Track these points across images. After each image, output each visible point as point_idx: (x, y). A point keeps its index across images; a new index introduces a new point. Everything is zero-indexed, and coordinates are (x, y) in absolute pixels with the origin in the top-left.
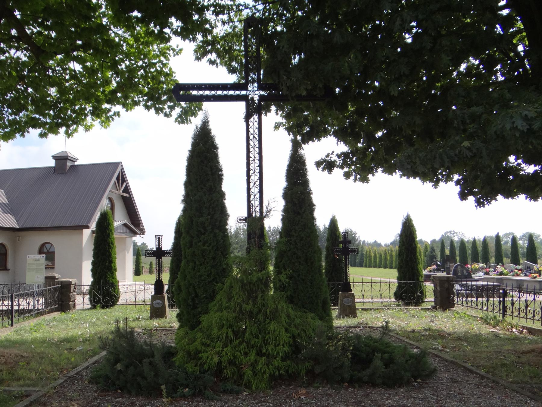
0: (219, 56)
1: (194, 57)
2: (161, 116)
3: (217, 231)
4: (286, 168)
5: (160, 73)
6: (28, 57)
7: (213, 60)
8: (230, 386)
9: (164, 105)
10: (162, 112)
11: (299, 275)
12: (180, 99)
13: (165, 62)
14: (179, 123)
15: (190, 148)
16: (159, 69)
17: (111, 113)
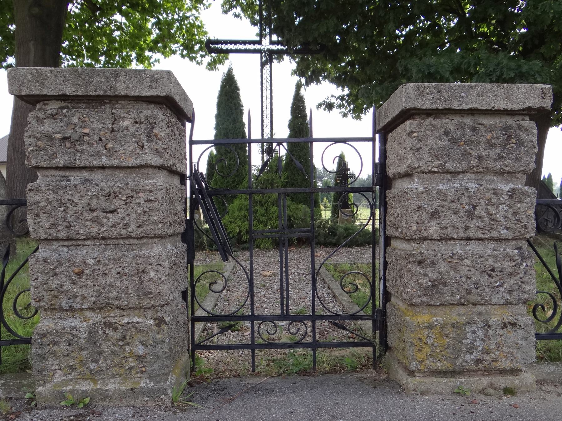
0: (243, 9)
1: (221, 11)
2: (194, 62)
3: (239, 151)
4: (291, 105)
5: (192, 25)
6: (79, 9)
7: (237, 14)
8: (247, 245)
9: (197, 54)
10: (195, 60)
11: (297, 183)
12: (211, 51)
13: (197, 15)
14: (209, 70)
15: (219, 89)
16: (192, 22)
17: (152, 60)
